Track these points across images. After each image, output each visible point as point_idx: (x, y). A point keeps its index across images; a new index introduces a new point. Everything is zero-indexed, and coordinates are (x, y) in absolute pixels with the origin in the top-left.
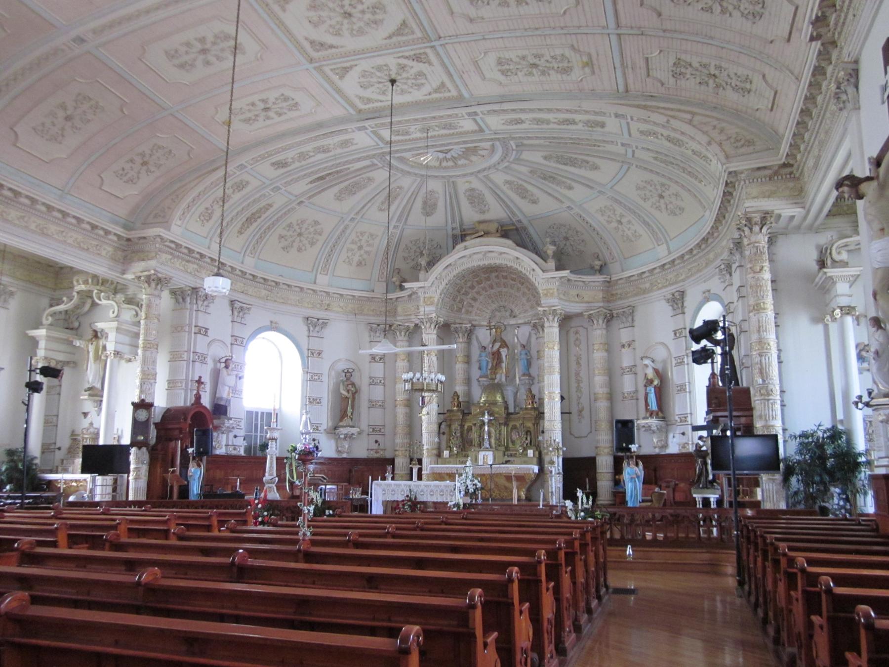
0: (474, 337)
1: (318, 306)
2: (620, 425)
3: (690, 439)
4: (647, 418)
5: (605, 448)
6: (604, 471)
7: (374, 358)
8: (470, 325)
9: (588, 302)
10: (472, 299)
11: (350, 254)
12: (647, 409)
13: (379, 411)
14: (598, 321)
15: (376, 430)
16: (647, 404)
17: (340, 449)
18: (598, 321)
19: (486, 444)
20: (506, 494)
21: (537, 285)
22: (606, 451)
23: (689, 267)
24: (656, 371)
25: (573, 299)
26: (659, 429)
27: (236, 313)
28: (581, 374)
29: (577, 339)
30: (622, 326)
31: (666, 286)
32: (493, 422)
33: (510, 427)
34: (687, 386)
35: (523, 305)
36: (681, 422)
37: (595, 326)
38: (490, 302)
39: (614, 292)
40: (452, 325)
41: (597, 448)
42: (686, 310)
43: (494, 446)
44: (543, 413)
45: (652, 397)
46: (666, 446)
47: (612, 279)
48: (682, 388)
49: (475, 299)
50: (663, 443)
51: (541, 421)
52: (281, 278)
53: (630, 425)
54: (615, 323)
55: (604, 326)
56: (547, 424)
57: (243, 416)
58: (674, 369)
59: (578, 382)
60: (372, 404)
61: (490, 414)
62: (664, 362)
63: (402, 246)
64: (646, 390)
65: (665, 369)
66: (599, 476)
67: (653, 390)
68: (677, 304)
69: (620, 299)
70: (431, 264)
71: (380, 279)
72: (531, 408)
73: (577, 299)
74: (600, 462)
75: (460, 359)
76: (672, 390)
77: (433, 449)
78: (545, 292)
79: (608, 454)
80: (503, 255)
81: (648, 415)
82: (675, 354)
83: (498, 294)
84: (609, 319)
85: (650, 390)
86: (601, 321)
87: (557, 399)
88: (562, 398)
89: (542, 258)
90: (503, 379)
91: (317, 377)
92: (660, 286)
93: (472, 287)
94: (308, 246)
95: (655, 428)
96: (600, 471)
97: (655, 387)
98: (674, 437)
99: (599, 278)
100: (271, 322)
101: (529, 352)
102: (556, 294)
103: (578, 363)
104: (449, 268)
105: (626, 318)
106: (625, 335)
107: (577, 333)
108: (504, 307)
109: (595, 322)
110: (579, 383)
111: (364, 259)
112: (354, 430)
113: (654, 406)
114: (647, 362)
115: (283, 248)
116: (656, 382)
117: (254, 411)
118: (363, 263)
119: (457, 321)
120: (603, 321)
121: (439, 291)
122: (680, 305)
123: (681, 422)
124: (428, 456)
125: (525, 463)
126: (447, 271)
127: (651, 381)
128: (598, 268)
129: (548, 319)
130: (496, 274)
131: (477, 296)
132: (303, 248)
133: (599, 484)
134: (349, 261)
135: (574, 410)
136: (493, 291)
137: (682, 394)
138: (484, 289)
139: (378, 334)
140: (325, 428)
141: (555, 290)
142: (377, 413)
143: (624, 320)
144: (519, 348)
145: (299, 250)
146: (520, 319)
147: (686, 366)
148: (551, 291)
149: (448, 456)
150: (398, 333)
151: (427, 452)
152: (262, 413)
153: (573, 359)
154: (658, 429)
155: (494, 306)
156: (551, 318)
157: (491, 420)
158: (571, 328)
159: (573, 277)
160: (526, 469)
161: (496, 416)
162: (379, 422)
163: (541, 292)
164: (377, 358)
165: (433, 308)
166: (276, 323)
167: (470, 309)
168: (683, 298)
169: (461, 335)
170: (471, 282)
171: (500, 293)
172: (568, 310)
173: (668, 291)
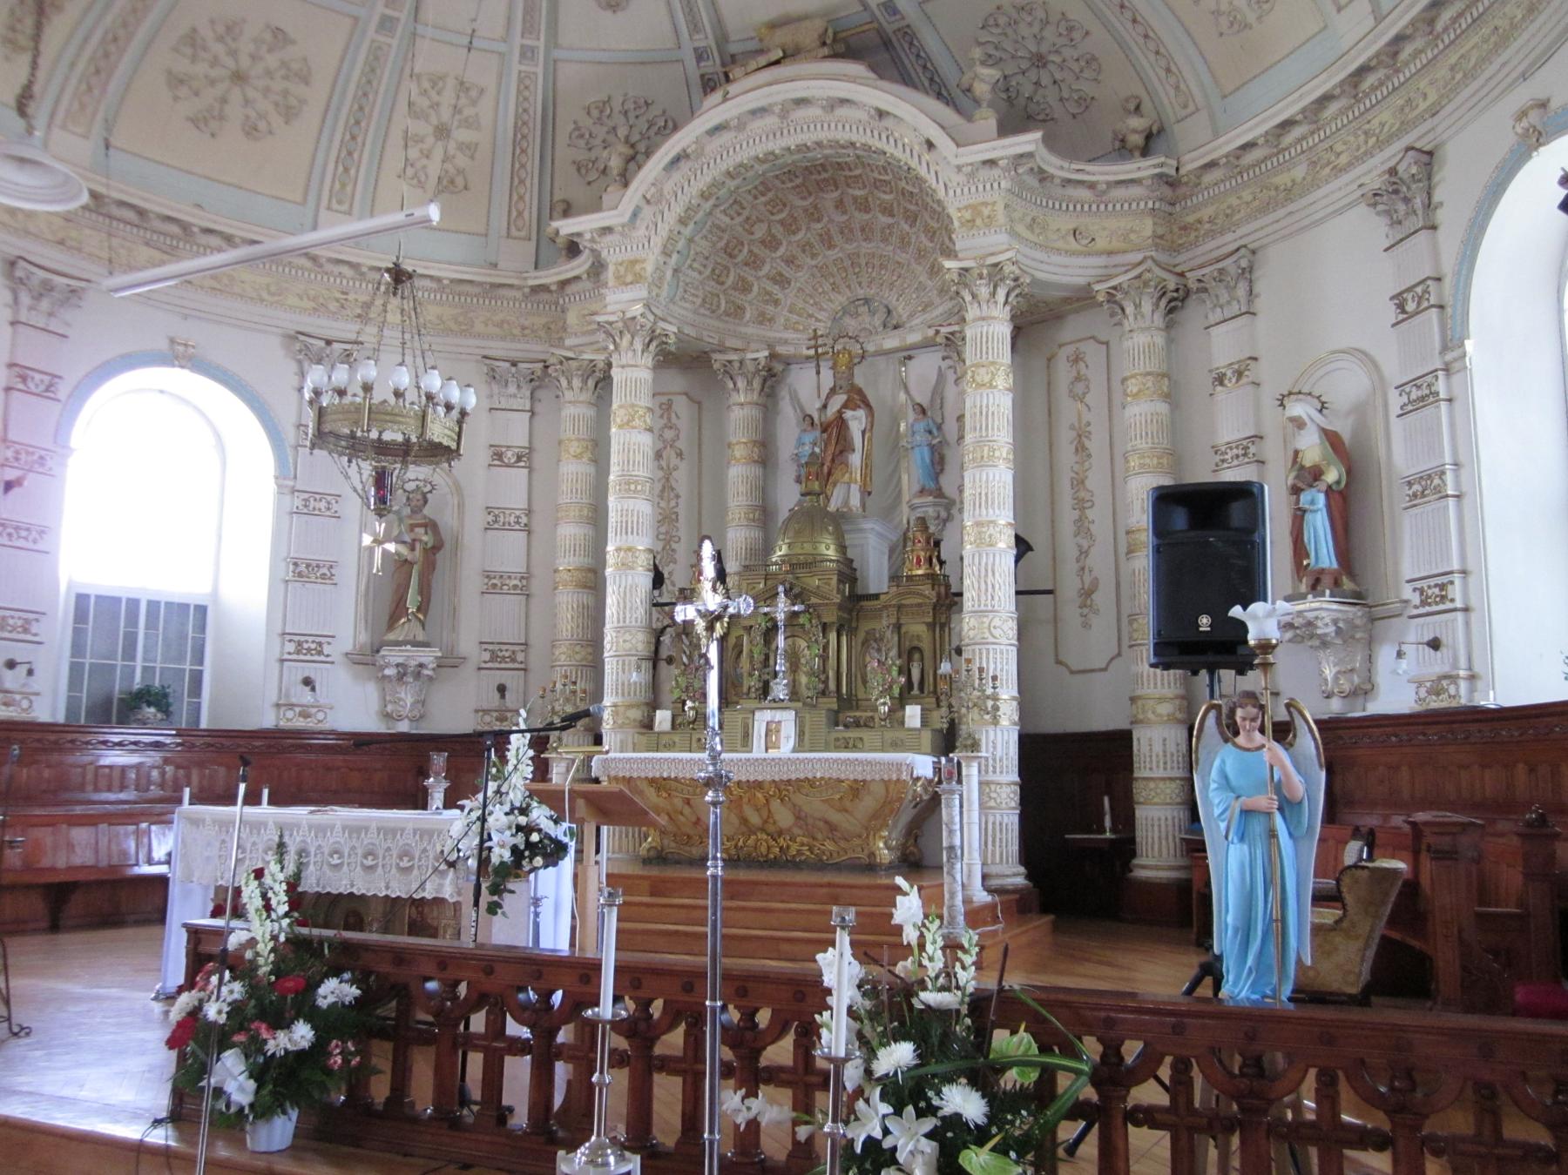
0: (784, 394)
1: (333, 306)
2: (1180, 519)
3: (1463, 662)
4: (1303, 597)
5: (1161, 700)
6: (1160, 773)
7: (499, 456)
8: (766, 353)
9: (1110, 253)
10: (774, 280)
11: (413, 153)
12: (1299, 569)
13: (514, 603)
14: (1138, 306)
15: (500, 655)
16: (1299, 550)
17: (389, 708)
18: (1138, 306)
19: (780, 689)
20: (829, 846)
21: (941, 194)
22: (1165, 709)
23: (1453, 59)
24: (1332, 439)
25: (1060, 244)
26: (1345, 633)
27: (25, 299)
28: (1089, 484)
29: (1078, 379)
30: (1217, 315)
31: (1369, 154)
32: (801, 620)
33: (861, 635)
34: (1449, 477)
35: (921, 287)
36: (1424, 603)
37: (1129, 324)
38: (827, 287)
39: (1190, 219)
40: (715, 356)
41: (1133, 700)
42: (1441, 216)
43: (804, 692)
44: (960, 594)
45: (1319, 526)
46: (1365, 690)
47: (1183, 171)
48: (1427, 487)
49: (781, 281)
50: (1356, 679)
51: (954, 617)
52: (196, 211)
53: (1237, 512)
54: (1194, 313)
55: (1159, 320)
56: (968, 625)
57: (63, 610)
58: (1397, 426)
59: (1081, 505)
60: (494, 584)
61: (794, 595)
62: (1360, 411)
63: (564, 129)
64: (1298, 501)
65: (1362, 428)
66: (1140, 791)
67: (1321, 499)
68: (1406, 200)
69: (1212, 234)
70: (635, 159)
71: (514, 232)
72: (926, 576)
73: (1074, 245)
74: (1145, 749)
75: (739, 452)
76: (1391, 496)
77: (630, 706)
78: (968, 215)
79: (1172, 719)
80: (842, 112)
81: (1303, 588)
82: (1395, 372)
83: (847, 263)
84: (1175, 302)
85: (1312, 502)
86: (1147, 306)
87: (1002, 545)
88: (1023, 546)
89: (958, 111)
90: (855, 501)
91: (323, 505)
92: (1344, 159)
93: (771, 243)
94: (277, 121)
95: (1331, 629)
96: (1147, 774)
97: (1329, 491)
98: (1400, 655)
99: (1143, 168)
100: (172, 341)
101: (939, 428)
102: (1001, 217)
103: (1081, 449)
104: (685, 166)
105: (1231, 289)
106: (1224, 345)
107: (1077, 359)
108: (867, 301)
109: (1130, 309)
110: (1083, 509)
111: (460, 172)
112: (428, 656)
113: (1324, 555)
114: (1298, 409)
115: (194, 121)
116: (1331, 476)
117: (124, 595)
118: (460, 181)
119: (730, 343)
120: (1157, 305)
121: (658, 241)
122: (1418, 203)
123: (1424, 603)
124: (618, 727)
125: (896, 746)
126: (677, 176)
127: (1316, 474)
128: (1136, 139)
129: (974, 296)
130: (836, 194)
131: (788, 272)
132: (262, 125)
133: (1140, 813)
134: (415, 176)
135: (1069, 587)
136: (833, 254)
137: (1428, 509)
138: (806, 247)
139: (512, 389)
140: (349, 647)
141: (1000, 207)
142: (507, 607)
143: (1224, 297)
144: (911, 416)
145: (251, 131)
146: (912, 330)
147: (1444, 406)
148: (986, 212)
149: (667, 726)
150: (564, 383)
151: (615, 714)
152: (153, 606)
153: (1065, 438)
154: (1339, 631)
155: (840, 300)
156: (984, 291)
157: (795, 614)
158: (1060, 346)
159: (1054, 165)
160: (890, 764)
161: (814, 600)
162: (512, 634)
163: (952, 211)
164: (510, 456)
165: (641, 292)
166: (193, 347)
167: (770, 309)
168: (1429, 178)
169: (741, 383)
170: (764, 226)
171: (854, 258)
172: (1040, 275)
173: (1371, 174)
